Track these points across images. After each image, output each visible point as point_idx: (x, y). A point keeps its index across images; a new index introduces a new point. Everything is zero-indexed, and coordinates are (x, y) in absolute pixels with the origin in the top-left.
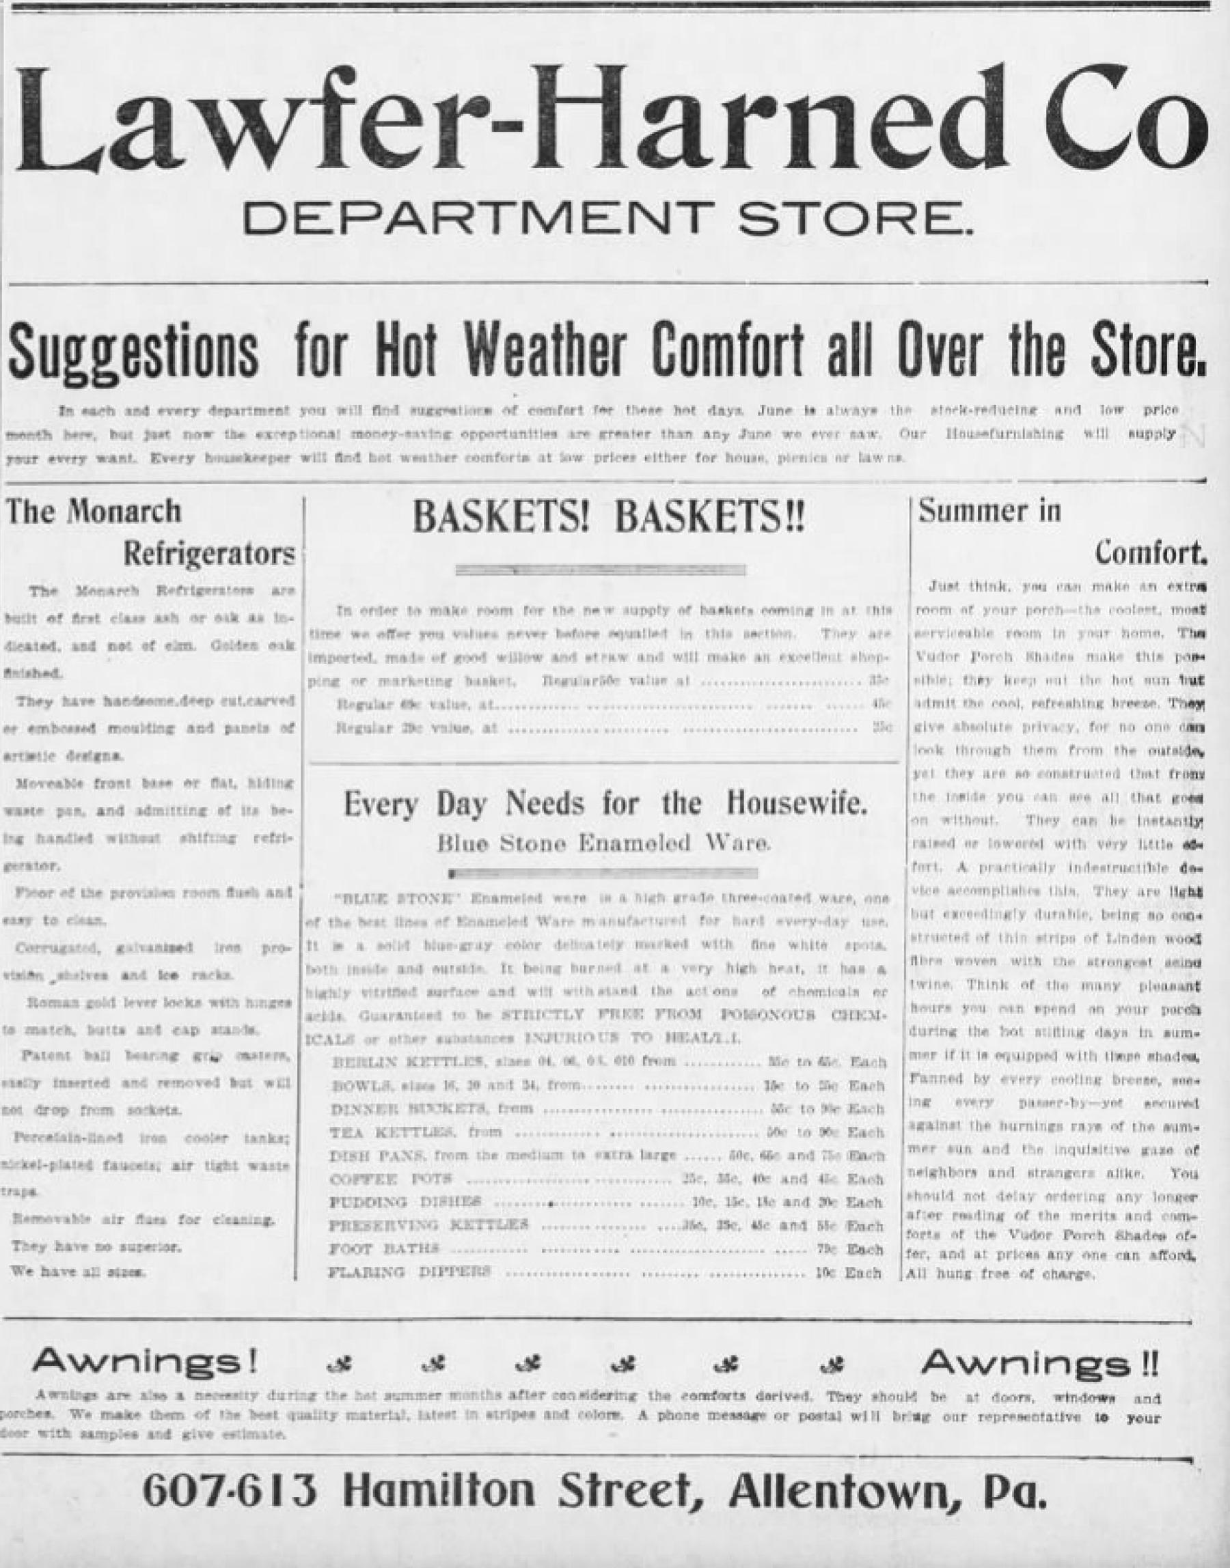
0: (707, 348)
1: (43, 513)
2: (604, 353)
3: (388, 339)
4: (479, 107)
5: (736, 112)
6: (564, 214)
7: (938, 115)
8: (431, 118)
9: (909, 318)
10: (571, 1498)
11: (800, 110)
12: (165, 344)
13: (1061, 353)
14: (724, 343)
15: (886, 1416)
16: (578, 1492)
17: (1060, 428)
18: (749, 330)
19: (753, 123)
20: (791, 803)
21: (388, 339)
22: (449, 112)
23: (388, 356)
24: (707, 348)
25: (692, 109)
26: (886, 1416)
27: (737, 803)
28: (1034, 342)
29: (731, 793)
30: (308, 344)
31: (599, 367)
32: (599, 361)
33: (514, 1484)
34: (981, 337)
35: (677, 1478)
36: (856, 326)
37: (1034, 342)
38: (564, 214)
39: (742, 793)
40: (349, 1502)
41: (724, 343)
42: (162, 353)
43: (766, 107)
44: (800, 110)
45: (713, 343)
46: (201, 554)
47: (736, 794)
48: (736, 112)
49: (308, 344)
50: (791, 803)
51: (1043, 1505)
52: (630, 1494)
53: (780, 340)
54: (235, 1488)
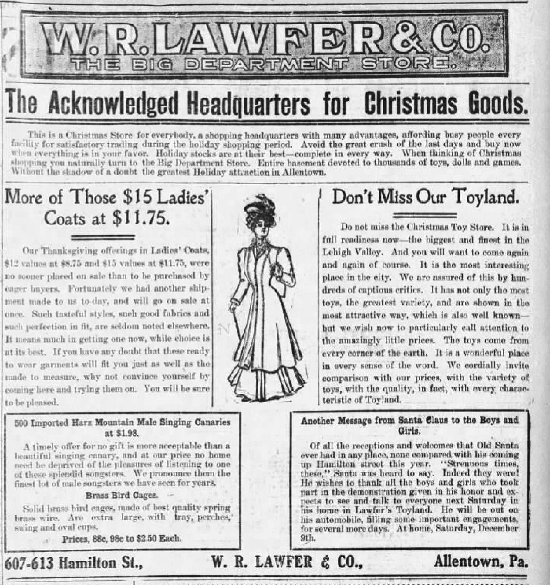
0: (96, 103)
2: (133, 104)
3: (193, 99)
6: (366, 46)
9: (36, 96)
12: (413, 101)
13: (35, 103)
14: (431, 101)
17: (439, 132)
18: (330, 96)
21: (193, 99)
23: (193, 105)
24: (96, 103)
28: (382, 101)
30: (330, 102)
31: (286, 111)
32: (286, 109)
34: (348, 99)
35: (83, 443)
37: (382, 101)
38: (366, 46)
41: (431, 101)
42: (412, 105)
45: (425, 102)
49: (330, 102)
53: (268, 100)
54: (30, 562)
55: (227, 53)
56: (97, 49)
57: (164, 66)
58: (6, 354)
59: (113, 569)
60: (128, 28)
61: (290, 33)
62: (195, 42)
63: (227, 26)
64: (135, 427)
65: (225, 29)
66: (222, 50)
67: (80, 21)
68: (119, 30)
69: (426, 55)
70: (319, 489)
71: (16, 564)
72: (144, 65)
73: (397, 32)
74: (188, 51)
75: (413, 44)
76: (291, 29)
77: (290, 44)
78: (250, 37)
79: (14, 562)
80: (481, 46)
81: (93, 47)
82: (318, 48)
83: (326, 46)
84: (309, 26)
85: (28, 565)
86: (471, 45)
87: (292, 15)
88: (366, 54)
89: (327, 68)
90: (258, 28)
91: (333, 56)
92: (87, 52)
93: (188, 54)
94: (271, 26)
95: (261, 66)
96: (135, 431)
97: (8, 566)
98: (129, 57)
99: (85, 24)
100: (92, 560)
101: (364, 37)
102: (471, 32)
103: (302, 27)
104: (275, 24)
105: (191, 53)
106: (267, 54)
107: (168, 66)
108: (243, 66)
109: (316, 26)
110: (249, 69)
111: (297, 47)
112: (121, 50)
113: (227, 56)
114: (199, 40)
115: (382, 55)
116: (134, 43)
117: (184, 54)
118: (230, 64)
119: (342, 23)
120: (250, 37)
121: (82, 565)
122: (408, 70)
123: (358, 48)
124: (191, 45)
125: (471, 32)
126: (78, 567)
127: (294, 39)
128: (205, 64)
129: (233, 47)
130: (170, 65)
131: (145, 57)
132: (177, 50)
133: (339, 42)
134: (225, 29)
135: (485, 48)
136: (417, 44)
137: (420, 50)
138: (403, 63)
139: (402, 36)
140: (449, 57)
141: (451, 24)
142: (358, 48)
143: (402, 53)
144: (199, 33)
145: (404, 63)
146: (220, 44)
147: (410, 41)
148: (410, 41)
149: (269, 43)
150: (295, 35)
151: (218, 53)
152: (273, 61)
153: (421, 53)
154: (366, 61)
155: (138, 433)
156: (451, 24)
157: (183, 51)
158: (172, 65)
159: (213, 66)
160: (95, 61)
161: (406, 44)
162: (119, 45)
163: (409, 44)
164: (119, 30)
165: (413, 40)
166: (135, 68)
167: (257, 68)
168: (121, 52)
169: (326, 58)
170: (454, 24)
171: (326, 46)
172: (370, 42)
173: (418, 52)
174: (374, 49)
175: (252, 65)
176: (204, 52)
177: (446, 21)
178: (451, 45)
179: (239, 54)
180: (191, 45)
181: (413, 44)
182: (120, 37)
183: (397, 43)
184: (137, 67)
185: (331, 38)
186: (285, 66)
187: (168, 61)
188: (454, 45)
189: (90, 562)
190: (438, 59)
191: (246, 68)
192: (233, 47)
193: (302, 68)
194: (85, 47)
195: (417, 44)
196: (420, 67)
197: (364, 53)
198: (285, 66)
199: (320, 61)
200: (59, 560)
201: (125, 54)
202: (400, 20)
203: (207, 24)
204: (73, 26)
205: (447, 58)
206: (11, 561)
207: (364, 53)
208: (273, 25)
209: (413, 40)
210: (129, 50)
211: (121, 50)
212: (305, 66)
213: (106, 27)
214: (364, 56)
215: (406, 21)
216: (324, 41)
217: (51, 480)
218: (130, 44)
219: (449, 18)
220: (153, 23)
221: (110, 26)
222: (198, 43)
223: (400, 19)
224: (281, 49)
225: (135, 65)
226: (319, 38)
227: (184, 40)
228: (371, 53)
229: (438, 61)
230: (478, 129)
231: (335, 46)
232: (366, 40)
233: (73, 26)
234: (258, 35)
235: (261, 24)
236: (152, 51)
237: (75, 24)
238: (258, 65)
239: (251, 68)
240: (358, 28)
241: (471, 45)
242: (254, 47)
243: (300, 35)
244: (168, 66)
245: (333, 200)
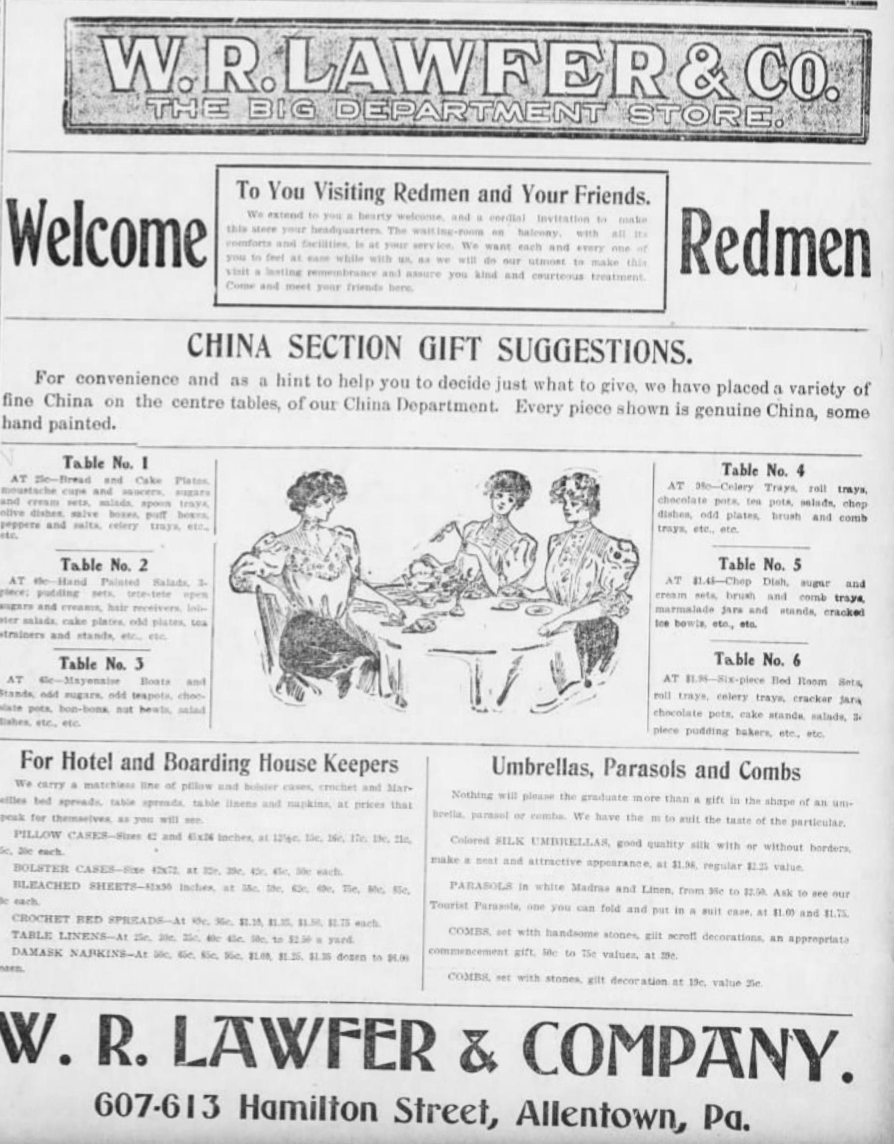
5: (632, 767)
6: (637, 85)
16: (409, 1113)
20: (306, 764)
25: (703, 768)
27: (69, 762)
29: (262, 755)
38: (637, 85)
39: (73, 753)
40: (243, 1115)
47: (266, 757)
48: (632, 767)
50: (658, 769)
55: (406, 92)
56: (272, 79)
57: (302, 112)
60: (652, 51)
61: (511, 57)
62: (354, 72)
63: (115, 42)
65: (112, 46)
66: (398, 88)
67: (457, 36)
68: (228, 48)
69: (734, 102)
72: (267, 109)
73: (689, 62)
74: (342, 86)
75: (715, 83)
76: (512, 51)
77: (510, 78)
78: (445, 63)
80: (825, 90)
81: (263, 81)
82: (558, 85)
83: (571, 82)
84: (543, 47)
85: (157, 1108)
86: (808, 88)
87: (850, 33)
88: (635, 97)
89: (572, 120)
90: (423, 47)
91: (582, 100)
92: (175, 87)
93: (341, 91)
94: (480, 45)
95: (462, 115)
98: (244, 96)
99: (172, 38)
100: (318, 1100)
101: (635, 68)
102: (809, 65)
103: (530, 48)
104: (487, 42)
105: (346, 91)
106: (474, 93)
107: (307, 113)
108: (432, 112)
109: (553, 46)
110: (442, 120)
111: (521, 82)
112: (230, 83)
113: (405, 96)
114: (360, 68)
115: (662, 101)
116: (252, 71)
117: (337, 91)
118: (409, 109)
119: (535, 42)
120: (445, 63)
121: (293, 1111)
122: (704, 128)
123: (624, 87)
124: (348, 77)
125: (809, 65)
127: (517, 67)
128: (369, 110)
129: (123, 77)
130: (311, 110)
131: (269, 96)
132: (323, 84)
133: (592, 76)
134: (112, 46)
135: (832, 94)
136: (721, 82)
137: (725, 94)
138: (698, 115)
139: (697, 69)
140: (771, 107)
141: (777, 51)
142: (624, 87)
143: (762, 98)
144: (360, 55)
145: (698, 115)
146: (394, 74)
147: (708, 76)
148: (708, 76)
149: (476, 76)
150: (519, 60)
151: (391, 91)
152: (481, 106)
153: (726, 98)
154: (637, 110)
156: (777, 51)
157: (333, 87)
158: (629, 112)
159: (381, 113)
160: (187, 102)
161: (702, 82)
162: (635, 79)
163: (709, 83)
164: (228, 48)
165: (714, 76)
166: (253, 115)
167: (456, 117)
168: (232, 87)
169: (570, 101)
170: (782, 51)
171: (571, 82)
172: (644, 76)
173: (721, 98)
174: (651, 90)
175: (446, 111)
176: (369, 89)
177: (769, 46)
178: (777, 85)
179: (425, 92)
180: (348, 77)
181: (715, 83)
182: (230, 61)
183: (688, 80)
184: (256, 112)
185: (580, 67)
186: (501, 114)
187: (308, 103)
188: (782, 86)
190: (754, 109)
191: (437, 117)
192: (415, 81)
193: (529, 118)
194: (171, 80)
195: (721, 82)
196: (723, 122)
197: (633, 95)
198: (501, 114)
199: (559, 107)
201: (239, 90)
202: (696, 41)
203: (374, 40)
204: (152, 41)
205: (768, 110)
207: (633, 95)
208: (482, 44)
209: (714, 76)
210: (244, 84)
211: (230, 83)
212: (372, 113)
213: (207, 42)
214: (632, 101)
215: (704, 43)
216: (568, 75)
218: (247, 73)
219: (774, 40)
220: (545, 40)
221: (212, 42)
222: (360, 73)
223: (692, 39)
224: (495, 85)
225: (253, 108)
226: (497, 68)
227: (336, 67)
228: (239, 90)
229: (753, 113)
231: (586, 82)
232: (636, 73)
233: (445, 44)
234: (422, 61)
235: (464, 41)
236: (281, 87)
237: (155, 38)
238: (729, 117)
239: (446, 117)
240: (625, 53)
241: (808, 88)
242: (452, 82)
243: (528, 61)
244: (307, 113)
245: (213, 302)
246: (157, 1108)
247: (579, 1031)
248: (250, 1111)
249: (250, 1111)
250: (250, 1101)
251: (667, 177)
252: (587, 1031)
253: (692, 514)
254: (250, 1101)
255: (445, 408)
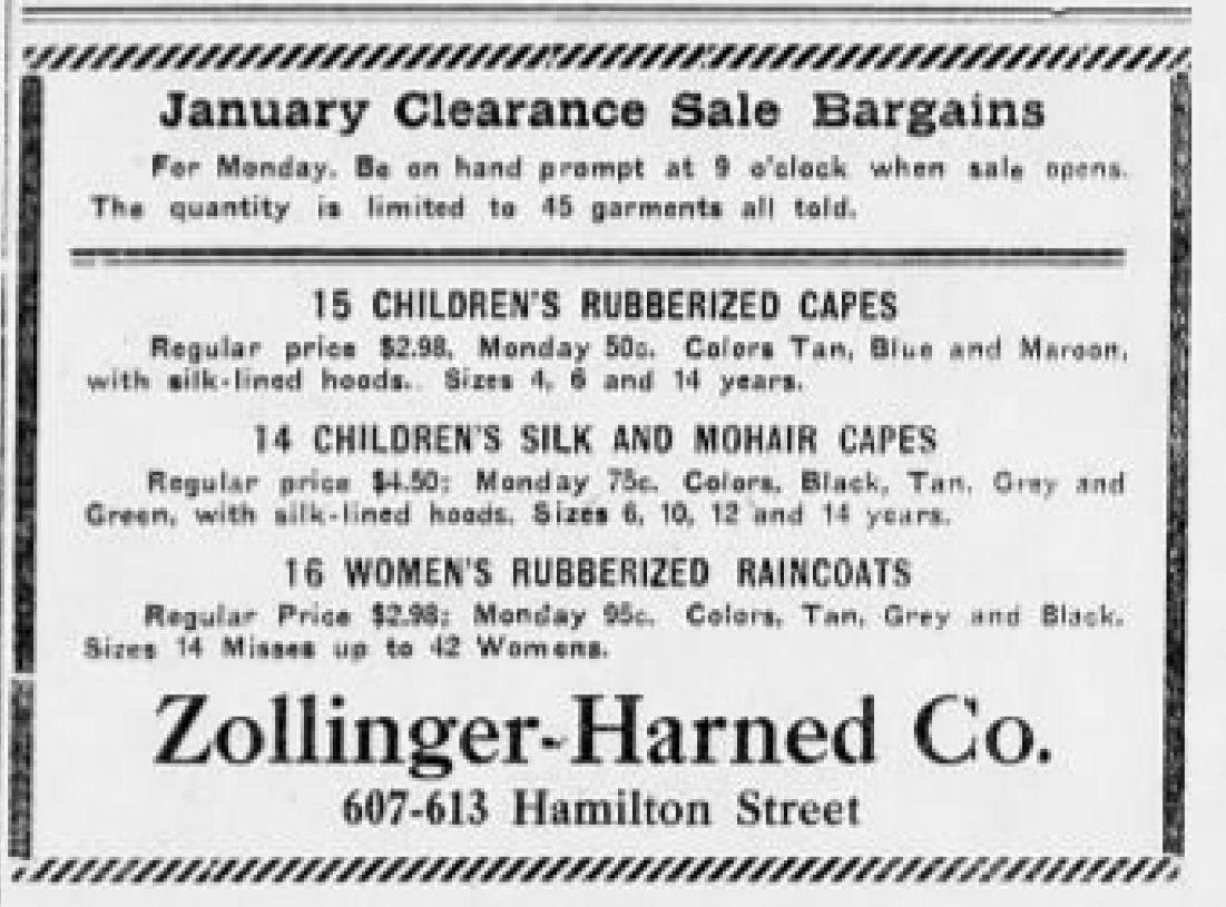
1: (793, 736)
4: (533, 723)
5: (703, 727)
7: (831, 732)
8: (505, 734)
10: (748, 816)
11: (743, 727)
15: (312, 380)
16: (756, 812)
19: (714, 734)
22: (515, 726)
26: (312, 380)
33: (692, 806)
36: (281, 704)
40: (520, 820)
43: (721, 723)
44: (743, 727)
46: (455, 734)
48: (703, 727)
51: (1045, 756)
52: (803, 814)
54: (422, 805)
58: (313, 343)
59: (699, 829)
64: (160, 192)
70: (815, 502)
71: (375, 808)
79: (369, 804)
85: (416, 813)
96: (441, 341)
97: (353, 814)
100: (628, 800)
121: (594, 815)
126: (579, 820)
155: (449, 346)
189: (621, 807)
200: (512, 801)
206: (361, 800)
217: (376, 638)
230: (642, 729)
246: (416, 813)
247: (1004, 730)
248: (530, 815)
249: (530, 815)
250: (530, 799)
251: (1181, 83)
252: (938, 745)
253: (968, 482)
254: (530, 799)
255: (855, 311)
